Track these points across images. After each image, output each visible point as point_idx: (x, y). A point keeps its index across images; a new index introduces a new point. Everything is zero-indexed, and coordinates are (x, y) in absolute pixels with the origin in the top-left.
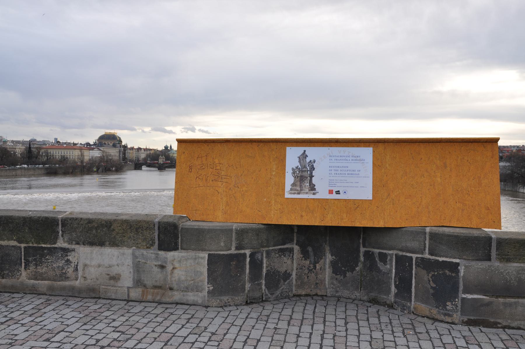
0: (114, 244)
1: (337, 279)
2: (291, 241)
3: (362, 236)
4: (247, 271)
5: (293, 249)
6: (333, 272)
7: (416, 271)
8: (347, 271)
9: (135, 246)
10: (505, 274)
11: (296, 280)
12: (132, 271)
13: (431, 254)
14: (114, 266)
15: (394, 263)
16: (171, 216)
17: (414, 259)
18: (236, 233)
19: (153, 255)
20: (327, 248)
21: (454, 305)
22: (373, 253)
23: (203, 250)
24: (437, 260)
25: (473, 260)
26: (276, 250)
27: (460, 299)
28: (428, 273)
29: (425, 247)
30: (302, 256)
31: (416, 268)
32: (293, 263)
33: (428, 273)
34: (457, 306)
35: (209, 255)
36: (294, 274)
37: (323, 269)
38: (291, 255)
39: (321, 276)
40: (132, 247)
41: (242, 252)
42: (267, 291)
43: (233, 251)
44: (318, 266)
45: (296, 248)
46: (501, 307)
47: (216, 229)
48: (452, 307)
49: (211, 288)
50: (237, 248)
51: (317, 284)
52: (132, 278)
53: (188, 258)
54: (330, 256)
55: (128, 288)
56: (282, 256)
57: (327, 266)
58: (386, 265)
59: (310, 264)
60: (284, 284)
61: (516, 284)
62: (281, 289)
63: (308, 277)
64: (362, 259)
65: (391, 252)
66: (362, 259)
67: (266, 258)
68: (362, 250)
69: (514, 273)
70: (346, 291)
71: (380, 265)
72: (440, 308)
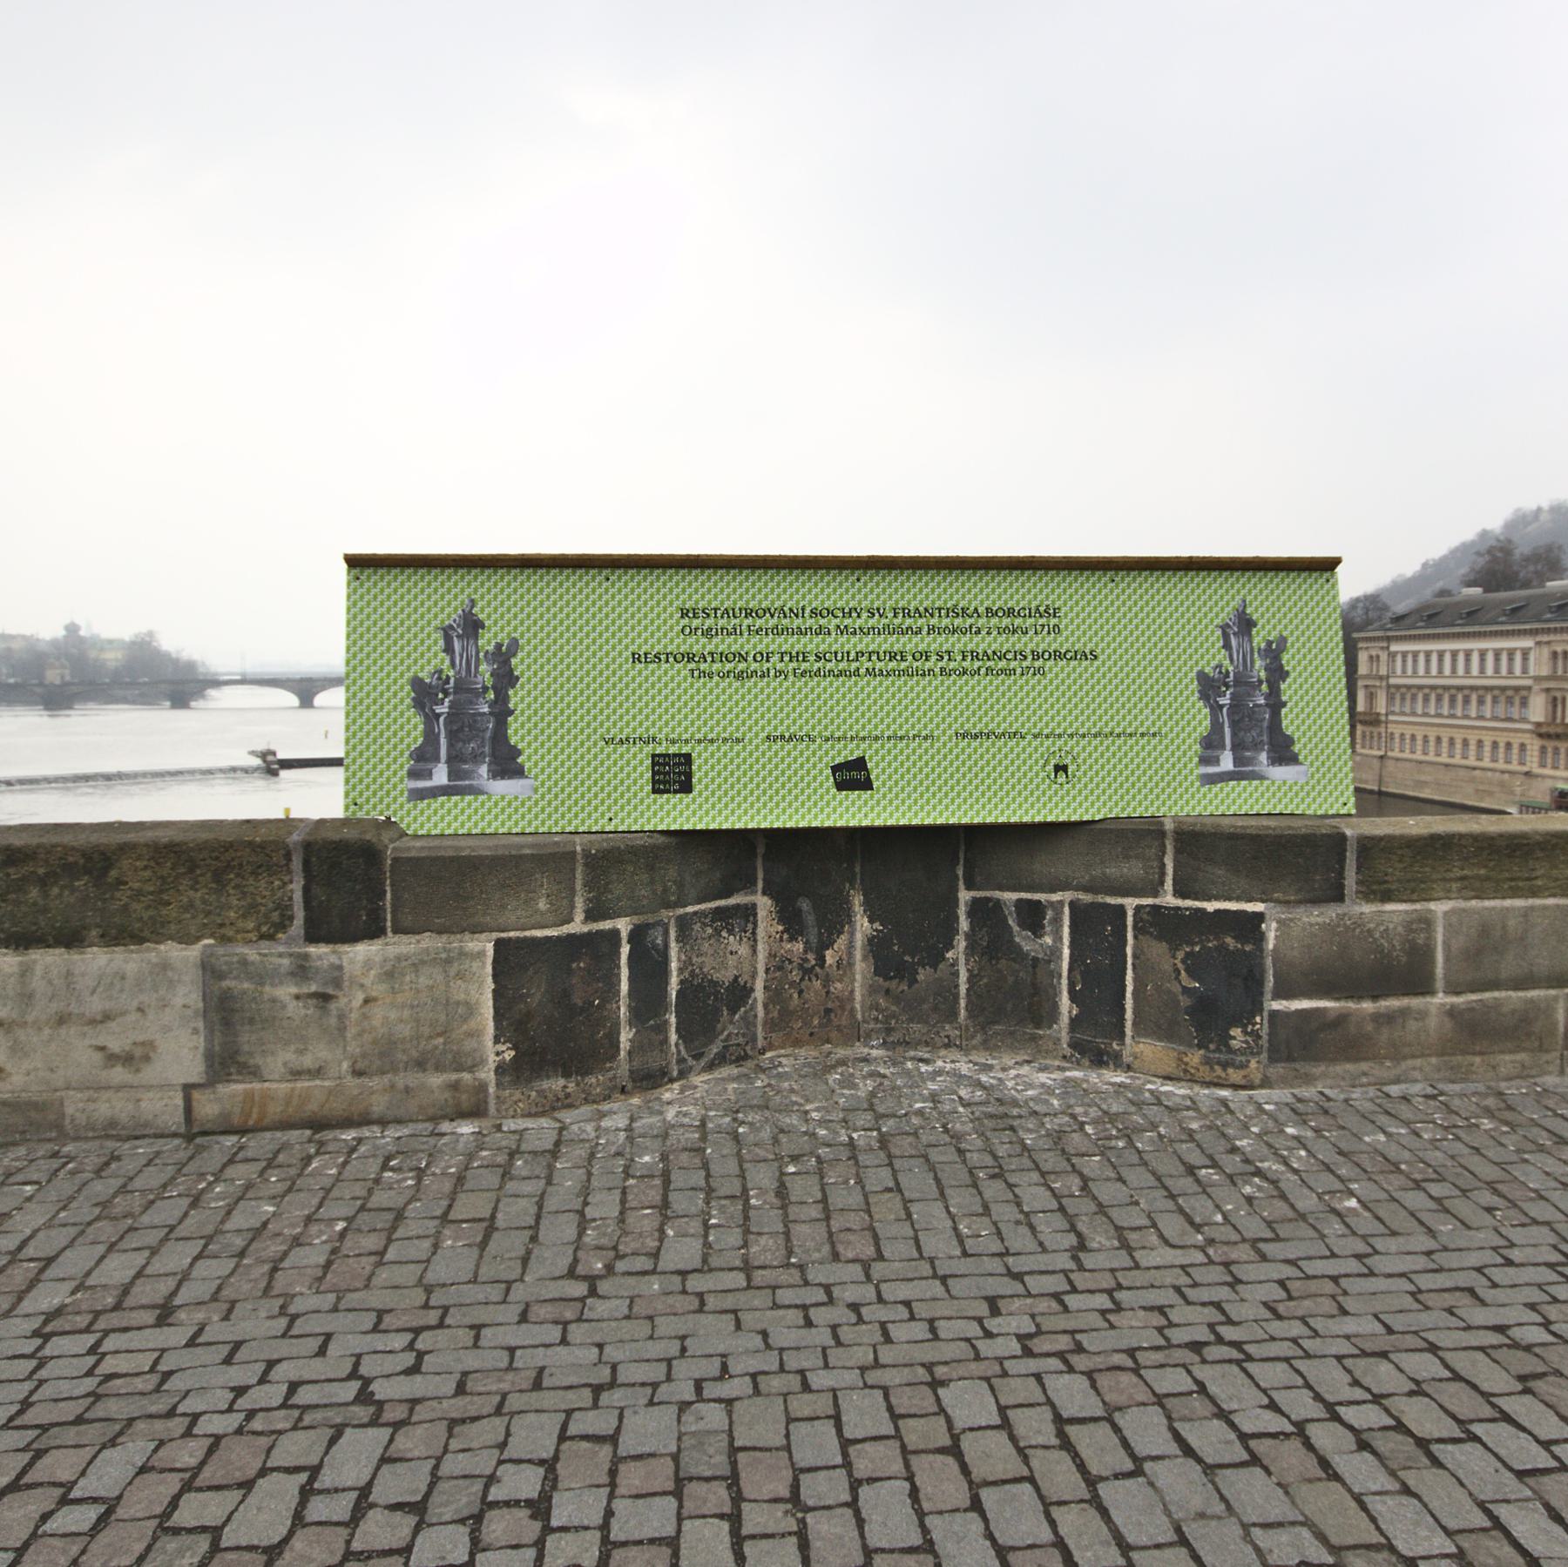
0: (121, 935)
1: (888, 991)
2: (748, 884)
3: (962, 855)
4: (624, 987)
5: (754, 906)
6: (876, 973)
7: (1135, 947)
8: (918, 964)
9: (212, 936)
10: (1377, 935)
11: (765, 1006)
12: (201, 1025)
13: (1180, 892)
14: (123, 1013)
15: (1066, 930)
16: (344, 822)
17: (1130, 913)
18: (586, 865)
19: (286, 961)
20: (857, 901)
21: (1249, 1034)
22: (998, 903)
23: (477, 929)
24: (1198, 910)
25: (1300, 902)
26: (702, 914)
27: (1265, 1014)
28: (1174, 949)
29: (1163, 874)
30: (781, 928)
31: (1135, 937)
32: (754, 951)
33: (1174, 949)
34: (1260, 1037)
35: (499, 944)
36: (759, 985)
37: (845, 965)
38: (750, 926)
39: (838, 985)
40: (198, 939)
41: (606, 925)
42: (682, 1048)
43: (577, 926)
44: (830, 957)
45: (764, 904)
46: (1369, 1027)
47: (521, 857)
48: (1246, 1042)
49: (509, 1055)
50: (590, 916)
51: (828, 1011)
52: (201, 1049)
53: (423, 962)
54: (866, 924)
55: (188, 1089)
56: (724, 934)
57: (858, 955)
58: (1041, 936)
59: (805, 952)
60: (731, 1022)
61: (1404, 959)
62: (722, 1037)
63: (800, 993)
64: (964, 924)
65: (1056, 897)
66: (964, 924)
67: (677, 941)
68: (964, 896)
69: (1400, 929)
70: (915, 1026)
71: (1024, 941)
72: (1212, 1046)
